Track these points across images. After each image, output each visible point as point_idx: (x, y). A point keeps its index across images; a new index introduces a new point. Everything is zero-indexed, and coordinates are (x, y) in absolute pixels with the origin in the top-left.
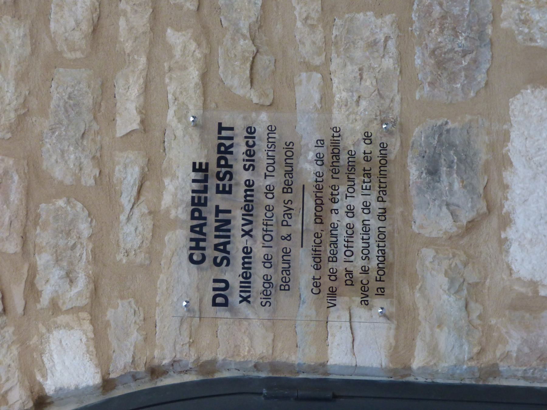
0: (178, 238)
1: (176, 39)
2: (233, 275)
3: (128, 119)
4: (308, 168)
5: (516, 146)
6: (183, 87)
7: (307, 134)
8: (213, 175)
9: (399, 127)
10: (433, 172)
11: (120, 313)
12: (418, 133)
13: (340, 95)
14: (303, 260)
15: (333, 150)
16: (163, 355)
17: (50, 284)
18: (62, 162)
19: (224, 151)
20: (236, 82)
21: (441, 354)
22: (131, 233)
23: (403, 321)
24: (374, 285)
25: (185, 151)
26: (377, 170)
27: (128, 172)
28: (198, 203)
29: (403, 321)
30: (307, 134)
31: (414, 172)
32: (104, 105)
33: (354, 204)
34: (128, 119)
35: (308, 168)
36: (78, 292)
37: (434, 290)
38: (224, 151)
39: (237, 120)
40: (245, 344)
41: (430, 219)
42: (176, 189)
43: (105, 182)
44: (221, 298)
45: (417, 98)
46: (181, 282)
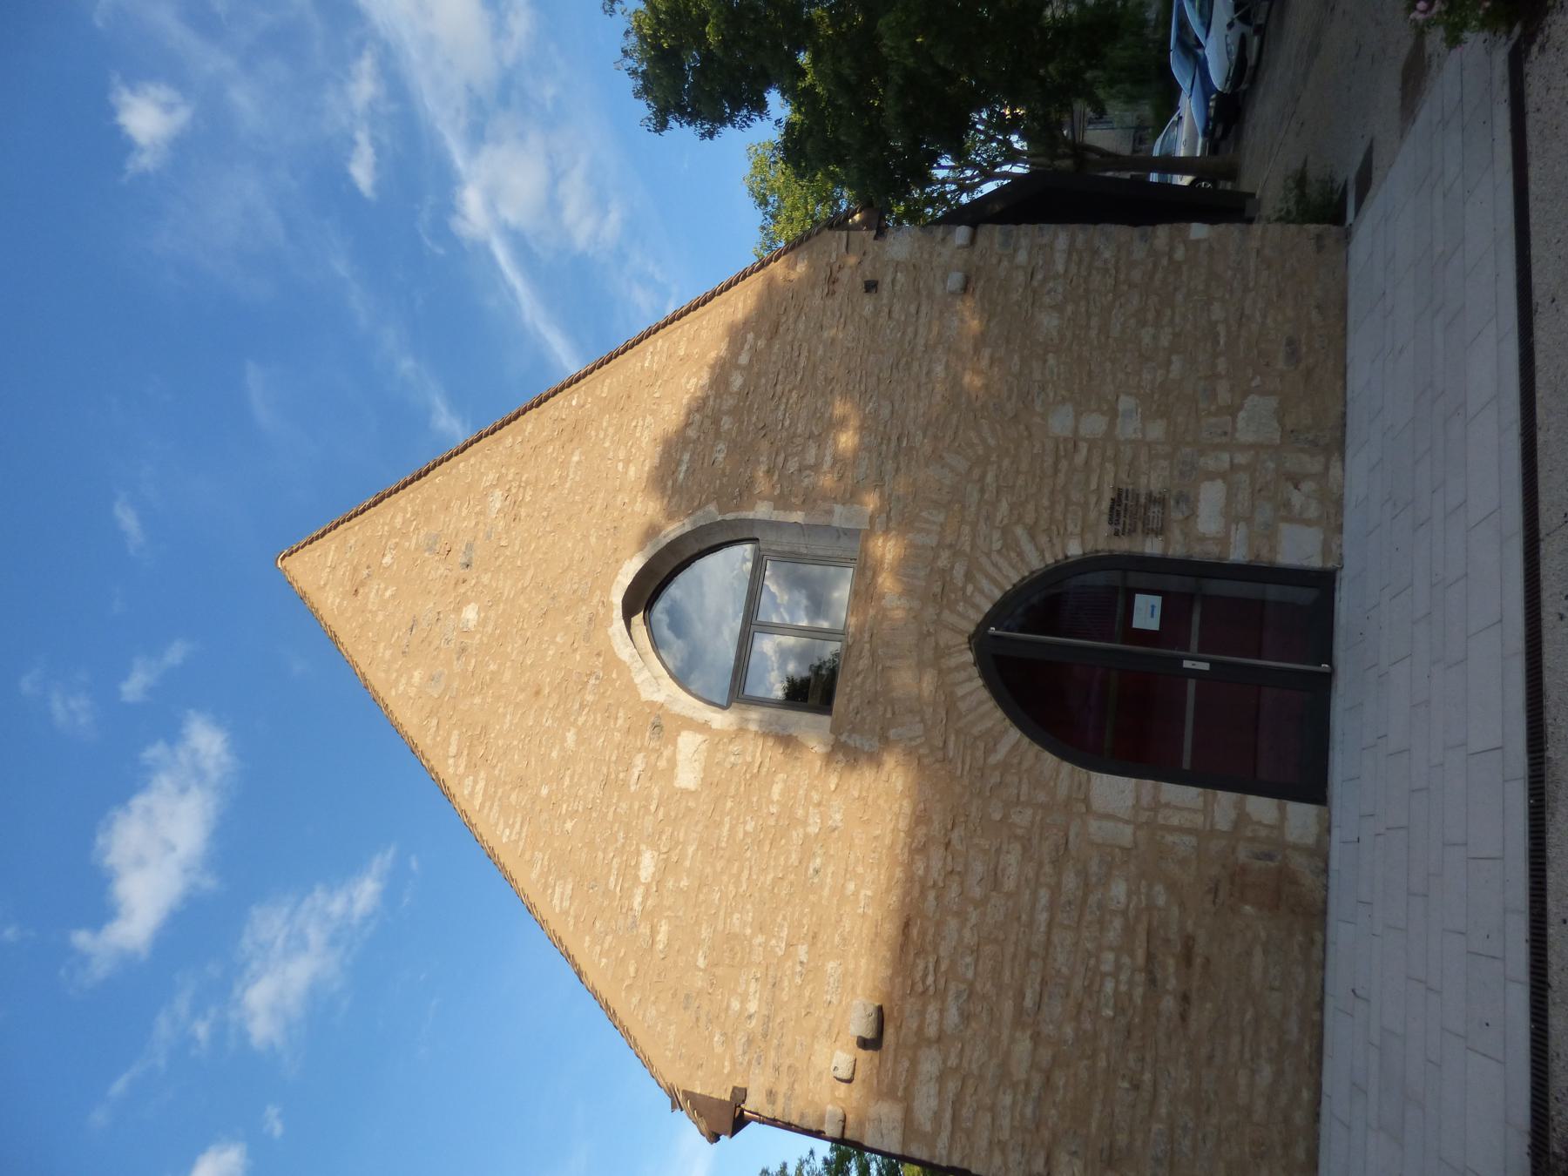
0: (1105, 518)
1: (1108, 465)
2: (1120, 528)
3: (1093, 486)
4: (1143, 500)
5: (1202, 496)
6: (1109, 480)
7: (1143, 492)
8: (1115, 502)
9: (1169, 491)
10: (1178, 503)
11: (1088, 536)
12: (1174, 492)
13: (1153, 480)
14: (1140, 525)
15: (1150, 495)
16: (1100, 547)
17: (1070, 528)
18: (1076, 496)
19: (1119, 495)
20: (1124, 476)
21: (1177, 550)
22: (1093, 515)
23: (1167, 543)
24: (1159, 532)
25: (1108, 495)
26: (1162, 502)
27: (1093, 499)
28: (1112, 508)
29: (1167, 543)
30: (1143, 492)
31: (1172, 502)
32: (1087, 482)
33: (1155, 511)
34: (1093, 486)
35: (1143, 500)
36: (1078, 530)
37: (1176, 533)
38: (1119, 495)
39: (1124, 487)
40: (1123, 545)
41: (1176, 515)
42: (1106, 505)
43: (1087, 503)
44: (1116, 534)
45: (272, 1111)
46: (1105, 529)
